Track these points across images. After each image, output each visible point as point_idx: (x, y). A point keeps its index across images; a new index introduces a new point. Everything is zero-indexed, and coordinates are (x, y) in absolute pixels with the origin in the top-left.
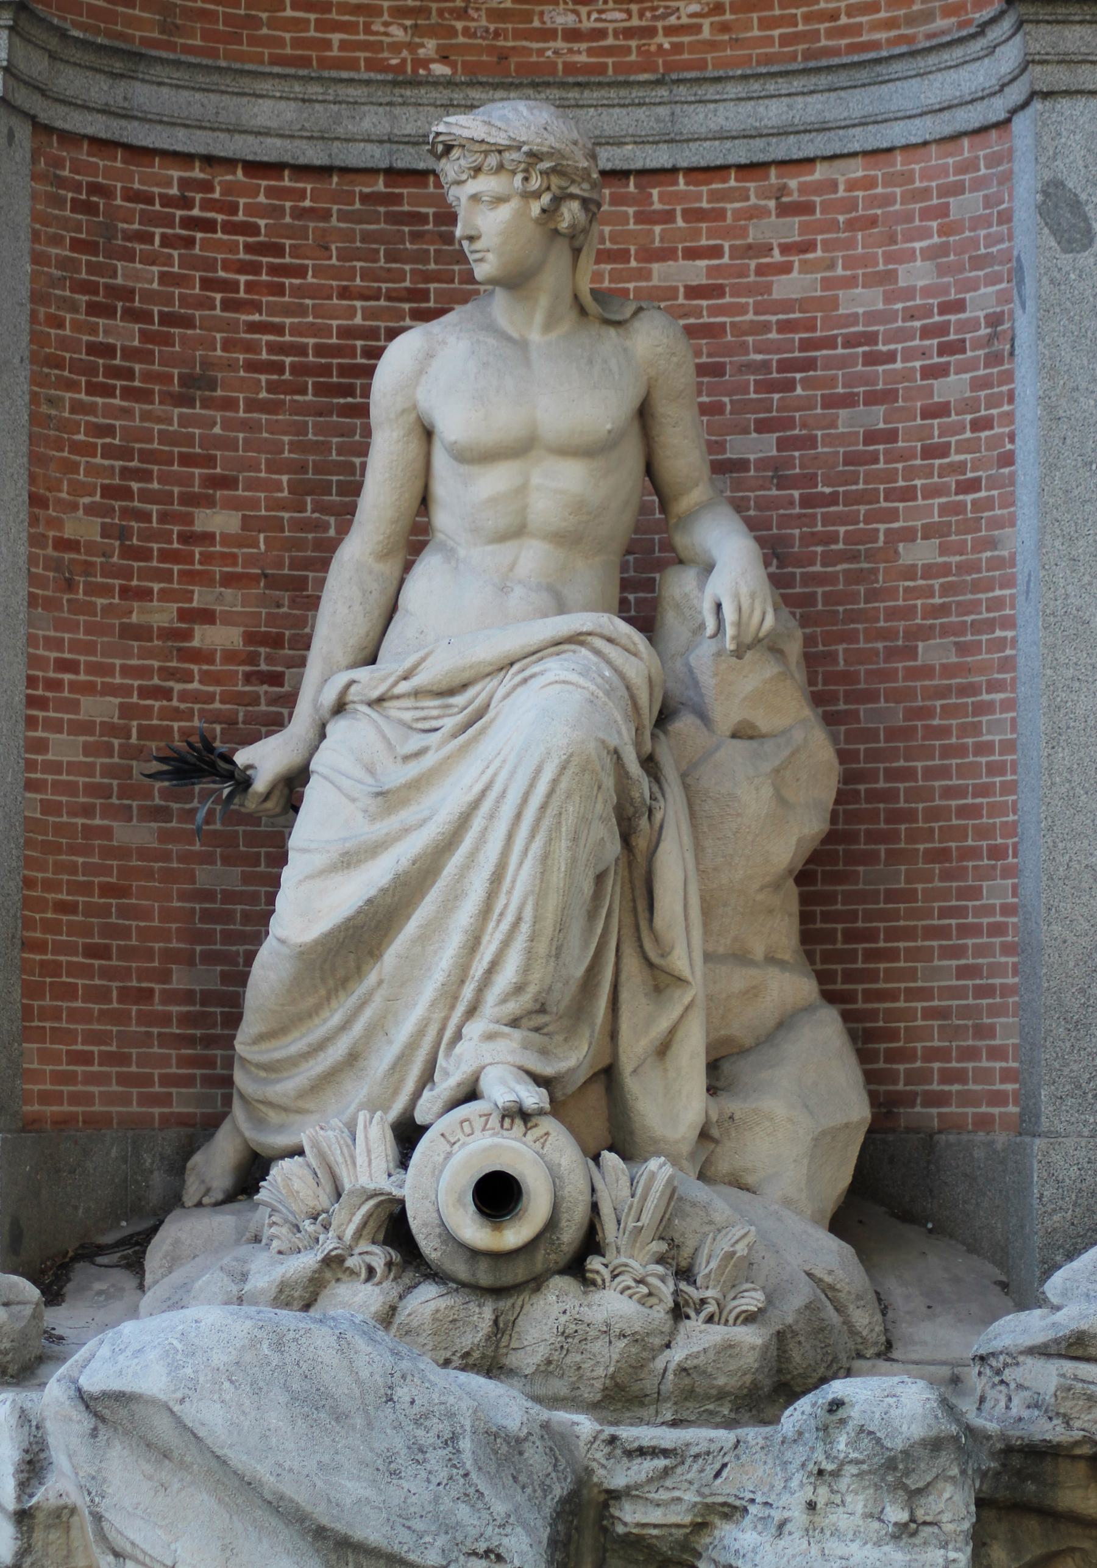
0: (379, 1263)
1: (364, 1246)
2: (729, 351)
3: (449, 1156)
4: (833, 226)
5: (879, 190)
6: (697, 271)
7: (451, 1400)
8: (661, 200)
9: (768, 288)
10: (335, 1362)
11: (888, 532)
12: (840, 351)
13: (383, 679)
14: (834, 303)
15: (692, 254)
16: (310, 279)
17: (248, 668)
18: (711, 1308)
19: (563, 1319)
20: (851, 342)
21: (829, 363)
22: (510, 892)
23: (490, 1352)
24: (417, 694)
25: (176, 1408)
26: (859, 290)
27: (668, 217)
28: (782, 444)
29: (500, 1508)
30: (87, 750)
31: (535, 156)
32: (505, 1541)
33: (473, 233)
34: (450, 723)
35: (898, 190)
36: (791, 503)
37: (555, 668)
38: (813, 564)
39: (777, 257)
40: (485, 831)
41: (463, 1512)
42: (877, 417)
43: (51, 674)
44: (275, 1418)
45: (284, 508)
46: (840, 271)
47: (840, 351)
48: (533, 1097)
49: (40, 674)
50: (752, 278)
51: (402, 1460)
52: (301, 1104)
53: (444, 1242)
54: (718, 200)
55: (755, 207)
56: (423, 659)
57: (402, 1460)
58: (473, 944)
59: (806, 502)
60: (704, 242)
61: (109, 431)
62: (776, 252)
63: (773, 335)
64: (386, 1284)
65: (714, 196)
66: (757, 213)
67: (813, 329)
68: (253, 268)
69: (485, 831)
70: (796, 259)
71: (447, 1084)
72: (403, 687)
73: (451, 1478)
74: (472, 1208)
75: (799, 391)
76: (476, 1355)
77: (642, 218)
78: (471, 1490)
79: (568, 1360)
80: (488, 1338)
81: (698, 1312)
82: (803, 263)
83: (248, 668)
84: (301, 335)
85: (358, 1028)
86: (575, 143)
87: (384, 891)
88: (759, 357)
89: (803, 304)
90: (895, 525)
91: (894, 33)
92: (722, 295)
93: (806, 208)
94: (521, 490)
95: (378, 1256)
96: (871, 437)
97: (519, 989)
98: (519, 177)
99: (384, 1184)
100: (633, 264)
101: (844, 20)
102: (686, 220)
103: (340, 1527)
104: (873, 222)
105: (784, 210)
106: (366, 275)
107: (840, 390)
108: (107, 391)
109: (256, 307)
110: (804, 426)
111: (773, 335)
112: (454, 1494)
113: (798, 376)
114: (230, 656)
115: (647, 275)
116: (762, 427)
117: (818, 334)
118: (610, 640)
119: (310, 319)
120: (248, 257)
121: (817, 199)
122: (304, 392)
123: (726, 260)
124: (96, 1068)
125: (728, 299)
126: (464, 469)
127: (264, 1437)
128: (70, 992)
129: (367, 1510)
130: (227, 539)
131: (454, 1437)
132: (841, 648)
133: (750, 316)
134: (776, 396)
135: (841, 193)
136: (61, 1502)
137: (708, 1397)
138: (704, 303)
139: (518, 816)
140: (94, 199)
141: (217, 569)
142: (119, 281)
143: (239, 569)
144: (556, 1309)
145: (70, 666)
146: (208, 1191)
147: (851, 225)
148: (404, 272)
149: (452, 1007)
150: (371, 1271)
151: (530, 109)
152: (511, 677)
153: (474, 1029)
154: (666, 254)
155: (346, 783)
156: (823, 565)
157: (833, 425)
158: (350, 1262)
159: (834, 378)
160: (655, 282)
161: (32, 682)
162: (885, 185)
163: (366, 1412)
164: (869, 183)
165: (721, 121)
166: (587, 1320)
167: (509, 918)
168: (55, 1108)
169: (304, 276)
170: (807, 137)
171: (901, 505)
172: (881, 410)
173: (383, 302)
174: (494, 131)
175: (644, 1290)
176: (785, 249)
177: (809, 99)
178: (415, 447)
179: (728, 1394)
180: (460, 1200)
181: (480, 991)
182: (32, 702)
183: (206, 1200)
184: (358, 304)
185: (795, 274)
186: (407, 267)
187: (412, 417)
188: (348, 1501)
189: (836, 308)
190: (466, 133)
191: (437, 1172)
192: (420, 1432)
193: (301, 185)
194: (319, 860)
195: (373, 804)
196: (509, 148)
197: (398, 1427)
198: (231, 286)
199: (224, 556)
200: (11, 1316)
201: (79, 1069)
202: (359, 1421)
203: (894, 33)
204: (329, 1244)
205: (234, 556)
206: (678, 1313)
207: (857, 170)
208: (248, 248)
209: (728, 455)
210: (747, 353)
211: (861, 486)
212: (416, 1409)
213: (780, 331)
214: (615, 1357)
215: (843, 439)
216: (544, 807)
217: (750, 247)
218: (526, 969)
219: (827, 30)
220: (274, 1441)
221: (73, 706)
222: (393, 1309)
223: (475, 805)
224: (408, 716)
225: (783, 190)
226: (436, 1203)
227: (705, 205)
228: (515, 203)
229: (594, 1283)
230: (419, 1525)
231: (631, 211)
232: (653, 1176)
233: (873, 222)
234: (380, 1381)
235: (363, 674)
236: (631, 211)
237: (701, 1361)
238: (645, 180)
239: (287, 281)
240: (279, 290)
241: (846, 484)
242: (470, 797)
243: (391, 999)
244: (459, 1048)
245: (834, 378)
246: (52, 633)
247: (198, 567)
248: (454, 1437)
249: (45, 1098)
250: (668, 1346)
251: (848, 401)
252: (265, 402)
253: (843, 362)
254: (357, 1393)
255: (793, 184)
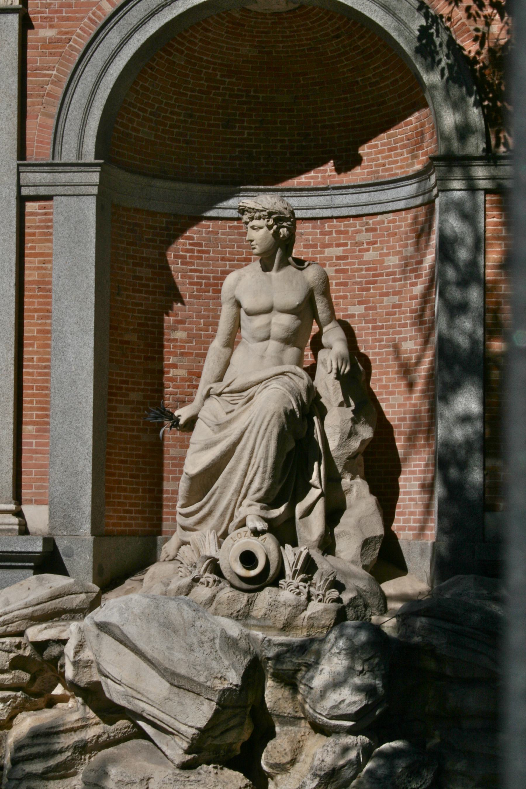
0: (211, 580)
1: (207, 574)
2: (349, 278)
3: (233, 545)
4: (383, 236)
5: (397, 223)
6: (339, 251)
7: (214, 626)
8: (328, 227)
9: (362, 256)
10: (176, 613)
11: (399, 338)
12: (385, 277)
13: (221, 387)
14: (383, 261)
15: (338, 245)
16: (211, 254)
17: (189, 383)
18: (321, 597)
19: (270, 600)
20: (388, 275)
21: (382, 282)
22: (256, 458)
23: (246, 611)
24: (231, 392)
25: (121, 627)
26: (391, 257)
27: (330, 233)
28: (366, 309)
29: (227, 663)
30: (132, 410)
31: (270, 214)
32: (228, 674)
33: (252, 239)
34: (241, 402)
35: (403, 223)
36: (369, 328)
37: (274, 384)
38: (375, 349)
39: (365, 246)
40: (249, 437)
41: (214, 664)
42: (395, 299)
43: (118, 385)
44: (154, 631)
45: (201, 330)
46: (385, 251)
47: (385, 277)
48: (261, 525)
49: (114, 385)
50: (357, 253)
51: (196, 645)
52: (195, 527)
53: (231, 574)
54: (347, 227)
55: (358, 230)
56: (234, 380)
57: (196, 645)
58: (245, 476)
59: (374, 328)
60: (342, 241)
61: (141, 305)
62: (365, 244)
63: (364, 272)
64: (213, 588)
65: (346, 226)
66: (358, 232)
67: (376, 270)
68: (192, 251)
69: (249, 437)
70: (371, 247)
71: (236, 521)
72: (227, 390)
73: (211, 652)
74: (239, 563)
75: (372, 291)
76: (242, 612)
77: (322, 233)
78: (218, 657)
79: (272, 614)
80: (246, 606)
81: (317, 598)
82: (374, 248)
83: (189, 383)
84: (208, 273)
85: (211, 502)
86: (286, 209)
87: (217, 457)
88: (359, 280)
89: (373, 262)
90: (401, 336)
91: (403, 170)
92: (347, 259)
93: (374, 230)
94: (269, 324)
95: (211, 577)
96: (394, 306)
97: (259, 490)
98: (266, 220)
99: (214, 554)
100: (319, 249)
101: (387, 166)
102: (336, 234)
103: (172, 668)
104: (395, 234)
105: (367, 230)
106: (230, 253)
107: (385, 291)
108: (140, 292)
109: (193, 264)
110: (373, 303)
111: (364, 272)
112: (212, 657)
113: (372, 286)
114: (183, 379)
115: (323, 253)
116: (360, 303)
117: (378, 272)
118: (295, 374)
119: (211, 268)
120: (190, 247)
121: (378, 227)
122: (209, 292)
123: (349, 247)
124: (133, 515)
125: (349, 260)
126: (250, 317)
127: (149, 638)
128: (125, 490)
129: (181, 662)
130: (182, 341)
131: (214, 639)
132: (384, 377)
133: (356, 266)
134: (364, 293)
135: (386, 225)
136: (88, 659)
137: (318, 627)
138: (342, 262)
139: (258, 432)
140: (136, 228)
141: (179, 351)
142: (144, 255)
143: (186, 351)
144: (268, 597)
145: (126, 382)
146: (168, 556)
147: (389, 235)
148: (243, 252)
149: (239, 496)
150: (208, 583)
151: (271, 197)
152: (261, 386)
153: (246, 502)
154: (329, 246)
155: (207, 421)
156: (379, 349)
157: (382, 302)
158: (201, 580)
159: (383, 287)
160: (326, 255)
161: (110, 387)
162: (399, 222)
163: (185, 630)
164: (394, 221)
165: (347, 201)
166: (279, 600)
167: (256, 466)
168: (119, 528)
169: (209, 253)
170: (375, 206)
171: (403, 329)
172: (397, 297)
173: (236, 262)
174: (257, 205)
175: (298, 591)
176: (368, 244)
177: (375, 193)
178: (234, 310)
179: (326, 626)
180: (236, 560)
181: (247, 490)
182: (110, 394)
183: (167, 559)
184: (228, 263)
185: (371, 252)
186: (244, 250)
187: (234, 300)
188: (176, 659)
189: (383, 263)
190: (249, 206)
191: (229, 550)
192: (203, 637)
193: (208, 223)
194: (198, 447)
195: (216, 428)
196: (262, 211)
197: (195, 635)
198: (185, 257)
199: (181, 346)
200: (87, 597)
201: (127, 515)
202: (182, 633)
203: (403, 170)
204: (195, 574)
205: (184, 346)
206: (309, 599)
207: (391, 216)
208: (190, 244)
209: (349, 313)
210: (355, 278)
211: (391, 323)
212: (202, 629)
213: (366, 271)
214: (288, 613)
215: (385, 307)
216: (266, 429)
217: (356, 243)
218: (262, 483)
219: (382, 170)
220: (152, 639)
221: (127, 395)
222: (215, 596)
223: (246, 429)
224: (228, 399)
225: (367, 224)
226: (228, 561)
227: (342, 229)
228: (265, 229)
229: (281, 588)
230: (199, 668)
231: (318, 231)
232: (301, 552)
233: (395, 234)
234: (191, 619)
235: (214, 385)
236: (318, 231)
237: (316, 615)
238: (323, 221)
239: (203, 255)
240: (200, 258)
241: (386, 322)
242: (244, 426)
243: (222, 493)
244: (240, 509)
245: (383, 287)
246: (118, 371)
247: (172, 350)
248: (214, 639)
249: (114, 525)
250: (306, 609)
251: (387, 294)
252: (196, 295)
253: (386, 281)
254: (182, 623)
255: (371, 222)
